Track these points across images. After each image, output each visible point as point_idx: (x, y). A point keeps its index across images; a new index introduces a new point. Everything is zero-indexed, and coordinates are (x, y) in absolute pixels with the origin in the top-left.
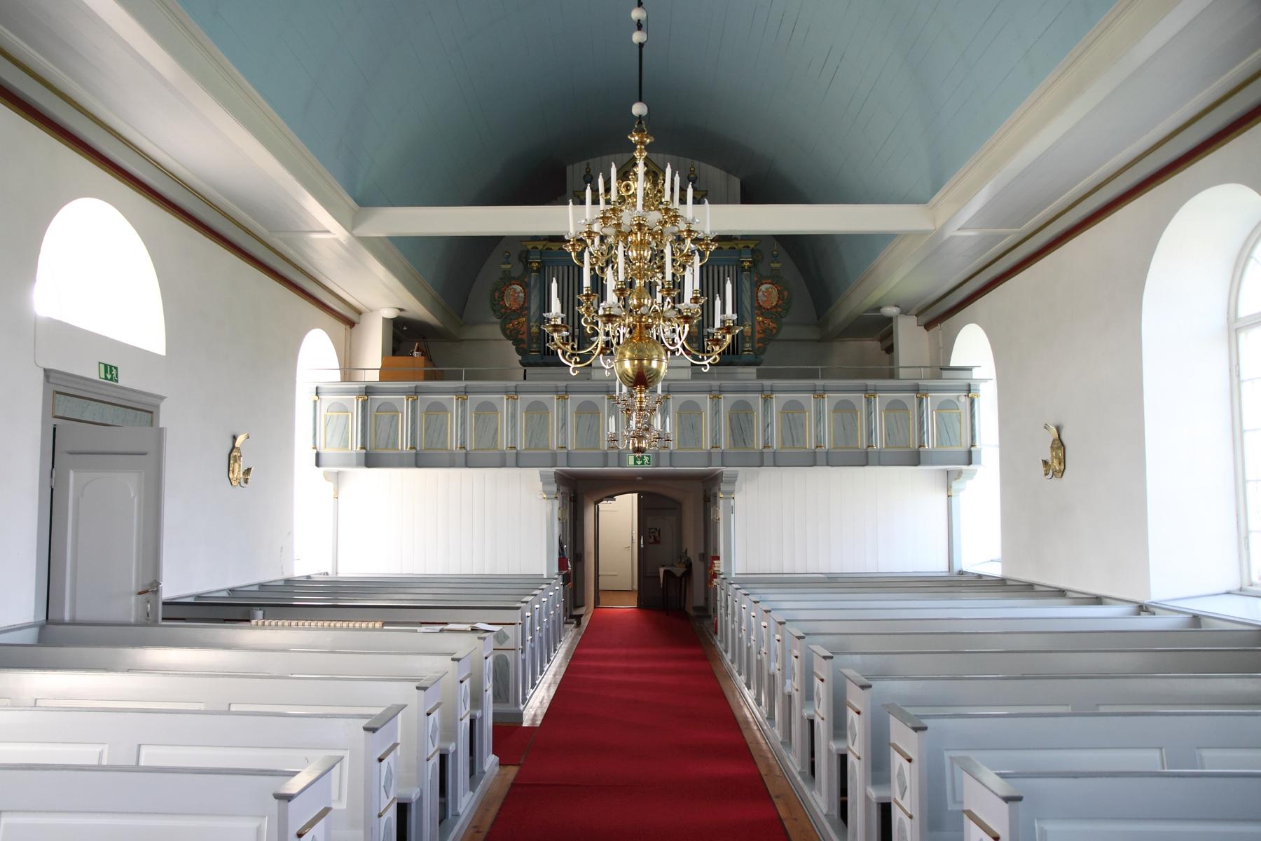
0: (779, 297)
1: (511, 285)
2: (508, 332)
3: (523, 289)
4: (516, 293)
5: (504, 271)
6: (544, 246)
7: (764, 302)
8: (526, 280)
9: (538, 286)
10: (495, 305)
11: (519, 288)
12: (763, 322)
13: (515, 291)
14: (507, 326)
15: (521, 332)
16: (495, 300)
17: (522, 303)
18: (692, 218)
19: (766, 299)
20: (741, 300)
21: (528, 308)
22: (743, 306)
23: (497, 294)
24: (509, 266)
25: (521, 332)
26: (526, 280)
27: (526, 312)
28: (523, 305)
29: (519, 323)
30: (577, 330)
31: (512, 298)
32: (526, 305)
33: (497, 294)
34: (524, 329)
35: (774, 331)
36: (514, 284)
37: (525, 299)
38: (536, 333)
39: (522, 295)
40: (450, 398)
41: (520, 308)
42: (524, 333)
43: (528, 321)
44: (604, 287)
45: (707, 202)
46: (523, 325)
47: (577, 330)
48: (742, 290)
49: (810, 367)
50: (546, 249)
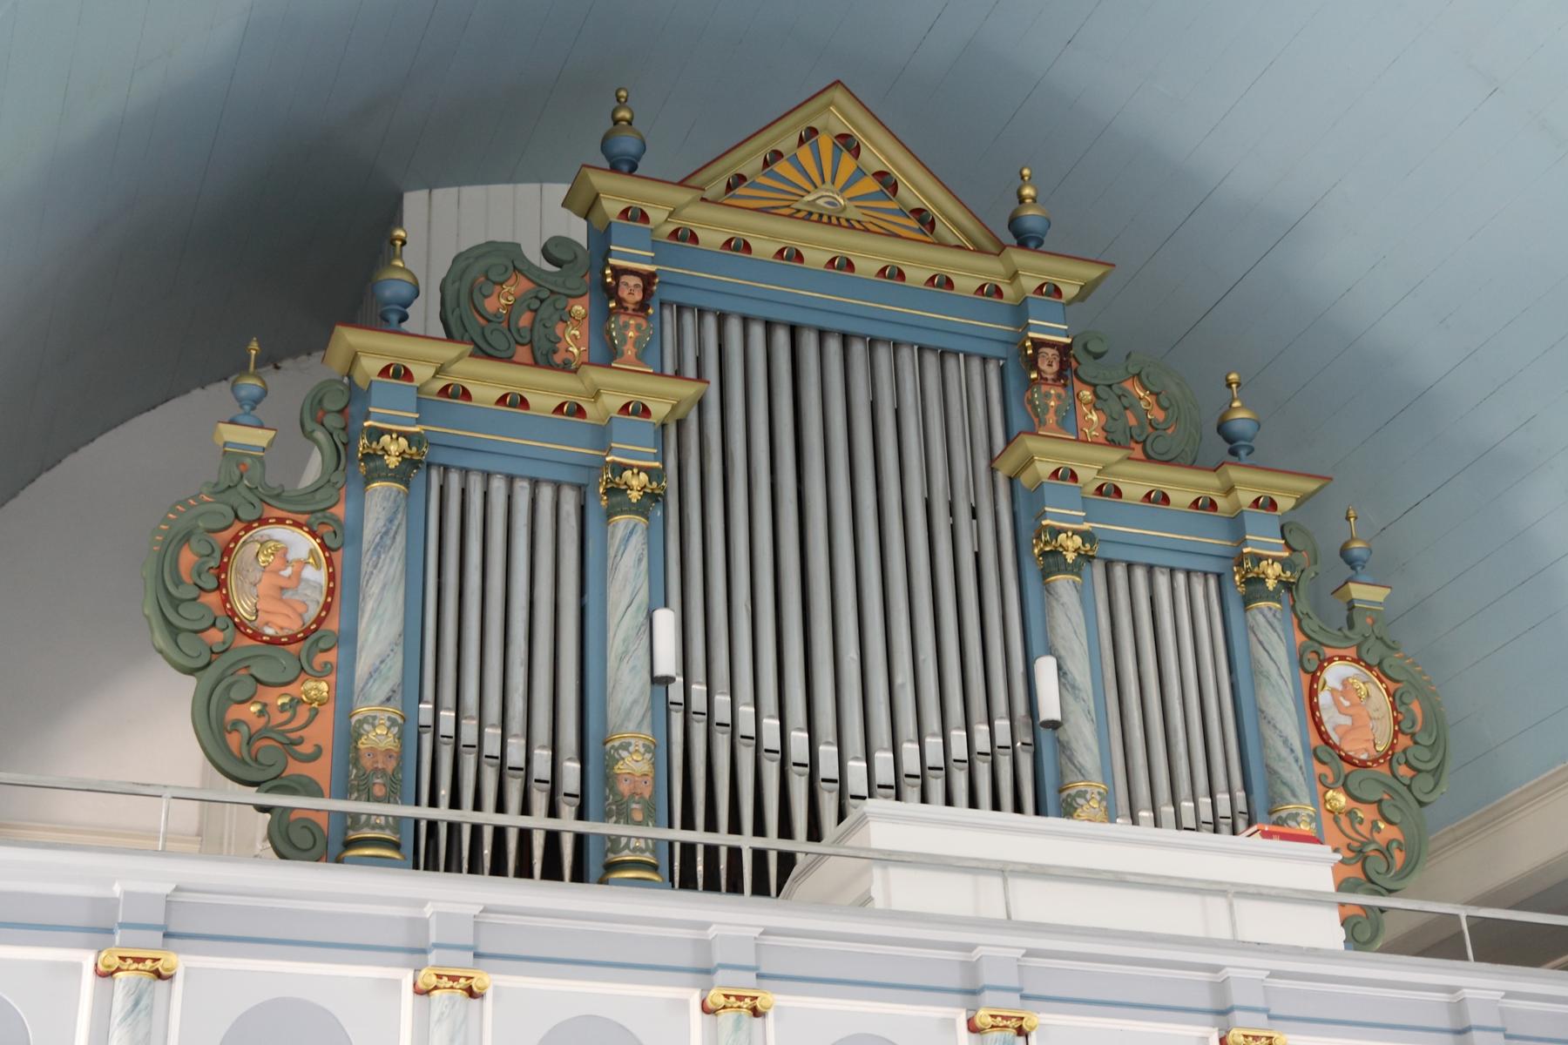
0: (1396, 721)
1: (263, 521)
2: (234, 740)
3: (324, 546)
4: (286, 563)
5: (233, 456)
6: (440, 371)
7: (1346, 732)
8: (339, 511)
9: (400, 540)
10: (176, 603)
11: (300, 543)
12: (1350, 813)
13: (282, 552)
14: (234, 712)
15: (306, 749)
16: (178, 582)
17: (313, 611)
18: (310, 430)
19: (1346, 721)
20: (1260, 712)
21: (348, 639)
22: (1269, 733)
23: (187, 558)
24: (261, 438)
25: (306, 749)
26: (339, 511)
27: (331, 657)
28: (319, 621)
29: (296, 702)
30: (571, 768)
31: (267, 581)
32: (333, 624)
33: (187, 558)
34: (321, 733)
35: (1399, 857)
36: (280, 521)
37: (331, 592)
38: (388, 753)
39: (317, 576)
40: (54, 966)
41: (308, 633)
42: (318, 753)
43: (345, 697)
44: (139, 963)
45: (650, 824)
46: (316, 712)
47: (571, 768)
48: (1256, 672)
49: (1000, 327)
50: (444, 391)
